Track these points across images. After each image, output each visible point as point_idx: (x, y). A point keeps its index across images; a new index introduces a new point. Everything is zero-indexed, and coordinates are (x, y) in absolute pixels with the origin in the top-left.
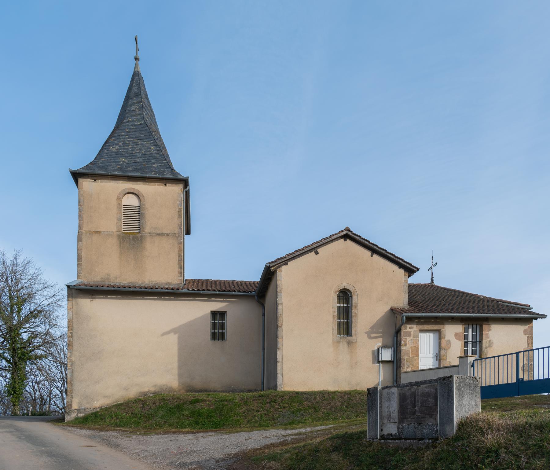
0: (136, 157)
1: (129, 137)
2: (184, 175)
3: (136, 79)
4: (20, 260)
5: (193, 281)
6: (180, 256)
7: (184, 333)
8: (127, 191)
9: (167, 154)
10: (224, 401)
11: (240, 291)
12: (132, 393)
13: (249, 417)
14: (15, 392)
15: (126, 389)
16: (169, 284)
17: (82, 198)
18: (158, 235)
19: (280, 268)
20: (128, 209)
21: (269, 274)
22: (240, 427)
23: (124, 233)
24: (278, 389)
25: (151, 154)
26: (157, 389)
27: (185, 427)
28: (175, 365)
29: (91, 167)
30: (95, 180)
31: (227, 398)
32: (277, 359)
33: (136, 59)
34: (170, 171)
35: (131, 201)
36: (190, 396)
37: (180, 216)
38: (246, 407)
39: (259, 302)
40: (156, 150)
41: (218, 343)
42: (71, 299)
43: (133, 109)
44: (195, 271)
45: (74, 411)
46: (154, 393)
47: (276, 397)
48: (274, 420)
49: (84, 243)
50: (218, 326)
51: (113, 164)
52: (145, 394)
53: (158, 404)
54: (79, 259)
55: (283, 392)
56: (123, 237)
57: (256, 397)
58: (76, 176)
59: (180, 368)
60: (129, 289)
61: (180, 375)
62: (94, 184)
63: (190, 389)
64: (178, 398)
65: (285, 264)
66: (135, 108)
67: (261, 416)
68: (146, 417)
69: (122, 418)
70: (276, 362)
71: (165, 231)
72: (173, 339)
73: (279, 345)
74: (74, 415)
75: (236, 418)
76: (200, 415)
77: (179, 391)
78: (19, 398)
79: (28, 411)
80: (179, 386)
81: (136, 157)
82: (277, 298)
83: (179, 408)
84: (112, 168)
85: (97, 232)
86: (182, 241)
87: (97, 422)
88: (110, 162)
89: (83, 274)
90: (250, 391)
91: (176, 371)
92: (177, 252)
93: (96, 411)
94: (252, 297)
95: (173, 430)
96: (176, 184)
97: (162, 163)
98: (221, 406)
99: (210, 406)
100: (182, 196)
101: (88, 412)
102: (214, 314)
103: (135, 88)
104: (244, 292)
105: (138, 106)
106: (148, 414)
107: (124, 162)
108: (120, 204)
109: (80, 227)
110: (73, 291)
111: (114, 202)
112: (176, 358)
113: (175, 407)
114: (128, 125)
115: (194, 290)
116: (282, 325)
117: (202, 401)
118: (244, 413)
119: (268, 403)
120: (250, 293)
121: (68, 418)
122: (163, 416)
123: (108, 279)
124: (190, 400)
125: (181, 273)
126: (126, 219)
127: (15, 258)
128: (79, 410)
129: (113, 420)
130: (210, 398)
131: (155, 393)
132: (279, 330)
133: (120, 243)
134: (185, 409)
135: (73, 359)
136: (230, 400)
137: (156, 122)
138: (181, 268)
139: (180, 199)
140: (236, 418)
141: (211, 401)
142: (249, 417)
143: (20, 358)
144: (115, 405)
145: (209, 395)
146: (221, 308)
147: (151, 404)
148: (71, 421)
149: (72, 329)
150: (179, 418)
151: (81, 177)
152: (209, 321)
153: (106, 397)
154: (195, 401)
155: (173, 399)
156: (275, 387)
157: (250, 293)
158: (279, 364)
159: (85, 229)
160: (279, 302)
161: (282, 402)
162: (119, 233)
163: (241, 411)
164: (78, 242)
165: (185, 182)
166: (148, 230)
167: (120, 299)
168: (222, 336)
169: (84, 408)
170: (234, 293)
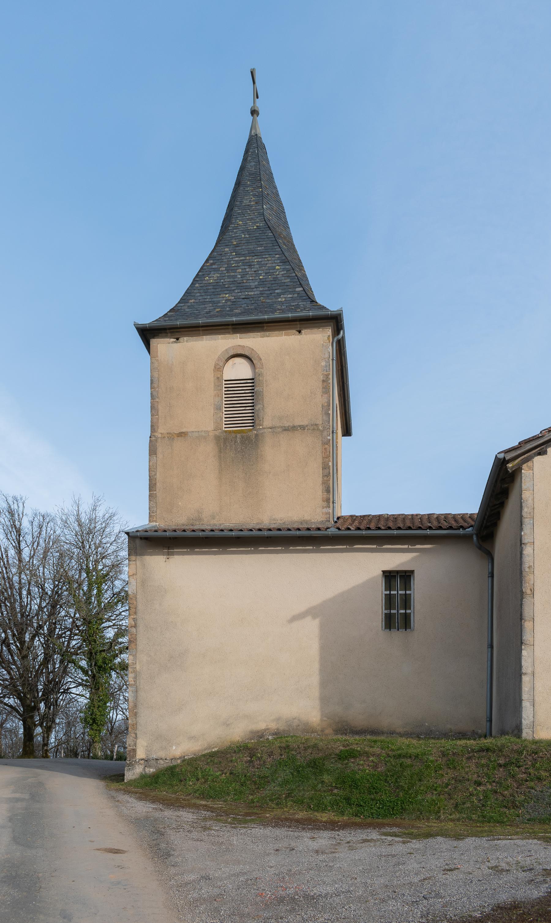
0: (249, 288)
1: (238, 255)
2: (332, 307)
3: (254, 148)
4: (100, 513)
5: (353, 518)
6: (325, 467)
7: (329, 614)
8: (232, 353)
9: (305, 276)
10: (405, 756)
11: (440, 528)
12: (237, 733)
13: (458, 797)
14: (94, 720)
15: (226, 724)
16: (306, 522)
17: (156, 375)
18: (286, 429)
19: (530, 463)
20: (233, 386)
21: (504, 480)
22: (438, 818)
23: (226, 432)
24: (524, 735)
25: (275, 279)
26: (281, 726)
27: (324, 810)
28: (315, 680)
29: (171, 316)
30: (178, 339)
31: (412, 751)
32: (520, 667)
33: (254, 112)
34: (308, 304)
35: (239, 370)
36: (338, 744)
37: (326, 390)
38: (451, 773)
39: (480, 548)
40: (284, 269)
41: (397, 635)
42: (133, 558)
43: (246, 202)
44: (358, 499)
45: (138, 763)
46: (276, 734)
47: (520, 753)
48: (515, 807)
49: (160, 455)
50: (398, 601)
51: (209, 307)
52: (260, 735)
53: (277, 757)
54: (152, 486)
55: (535, 742)
56: (225, 440)
57: (473, 751)
58: (148, 334)
59: (323, 684)
60: (230, 533)
61: (324, 700)
62: (176, 345)
63: (344, 728)
64: (315, 746)
65: (539, 454)
66: (249, 200)
67: (486, 797)
68: (255, 783)
69: (213, 781)
70: (518, 674)
71: (298, 422)
72: (311, 628)
73: (527, 637)
74: (138, 770)
75: (429, 797)
76: (355, 784)
77: (322, 731)
78: (100, 731)
79: (112, 752)
80: (322, 720)
81: (249, 288)
82: (521, 530)
83: (316, 766)
84: (207, 313)
85: (182, 434)
86: (330, 438)
87: (172, 786)
88: (204, 303)
89: (158, 512)
90: (462, 735)
91: (316, 692)
92: (320, 460)
93: (174, 763)
94: (466, 538)
95: (300, 815)
96: (319, 327)
97: (294, 292)
98: (398, 768)
99: (375, 767)
100: (330, 350)
101: (162, 764)
102: (390, 576)
103: (251, 166)
104: (451, 528)
105: (254, 195)
106: (259, 777)
107: (227, 300)
108: (219, 379)
109: (153, 428)
110: (138, 541)
111: (210, 376)
112: (316, 666)
113: (308, 765)
114: (236, 233)
115: (349, 529)
116: (533, 591)
117: (360, 755)
118: (447, 785)
119: (500, 766)
120: (461, 531)
121: (129, 775)
122: (286, 782)
123: (200, 519)
124: (337, 752)
125: (328, 500)
126: (230, 406)
127: (94, 510)
128: (147, 761)
129: (198, 784)
130: (377, 750)
131: (277, 734)
132: (527, 601)
133: (220, 452)
134: (327, 770)
135: (138, 667)
136: (417, 756)
137: (286, 222)
138: (328, 491)
139: (327, 356)
140: (429, 797)
141: (379, 756)
142: (458, 797)
143: (100, 667)
144: (204, 756)
145: (375, 742)
146: (402, 564)
147: (265, 757)
148: (135, 780)
149: (135, 613)
150: (314, 788)
151: (154, 337)
152: (379, 591)
153: (192, 738)
154: (348, 755)
155: (305, 749)
156: (518, 730)
157: (461, 531)
158: (526, 679)
159: (162, 430)
160: (526, 540)
161: (533, 766)
162: (217, 433)
163: (439, 782)
164: (150, 455)
165: (335, 321)
166: (267, 421)
167: (215, 553)
168: (406, 622)
169: (155, 757)
170: (429, 532)
